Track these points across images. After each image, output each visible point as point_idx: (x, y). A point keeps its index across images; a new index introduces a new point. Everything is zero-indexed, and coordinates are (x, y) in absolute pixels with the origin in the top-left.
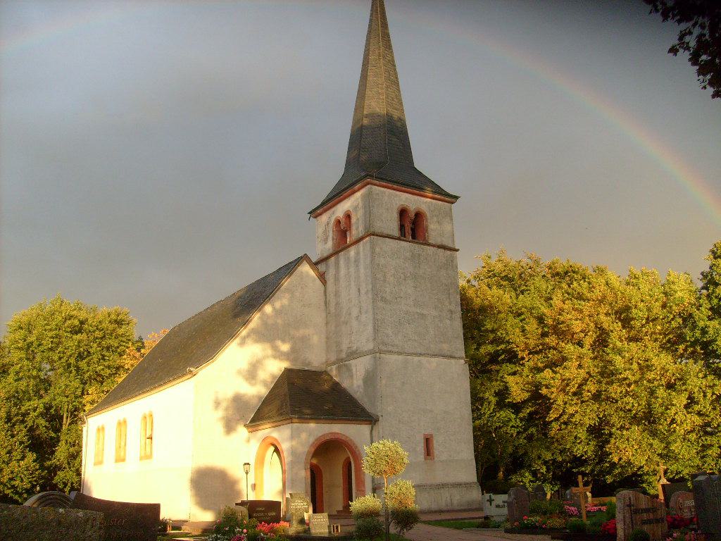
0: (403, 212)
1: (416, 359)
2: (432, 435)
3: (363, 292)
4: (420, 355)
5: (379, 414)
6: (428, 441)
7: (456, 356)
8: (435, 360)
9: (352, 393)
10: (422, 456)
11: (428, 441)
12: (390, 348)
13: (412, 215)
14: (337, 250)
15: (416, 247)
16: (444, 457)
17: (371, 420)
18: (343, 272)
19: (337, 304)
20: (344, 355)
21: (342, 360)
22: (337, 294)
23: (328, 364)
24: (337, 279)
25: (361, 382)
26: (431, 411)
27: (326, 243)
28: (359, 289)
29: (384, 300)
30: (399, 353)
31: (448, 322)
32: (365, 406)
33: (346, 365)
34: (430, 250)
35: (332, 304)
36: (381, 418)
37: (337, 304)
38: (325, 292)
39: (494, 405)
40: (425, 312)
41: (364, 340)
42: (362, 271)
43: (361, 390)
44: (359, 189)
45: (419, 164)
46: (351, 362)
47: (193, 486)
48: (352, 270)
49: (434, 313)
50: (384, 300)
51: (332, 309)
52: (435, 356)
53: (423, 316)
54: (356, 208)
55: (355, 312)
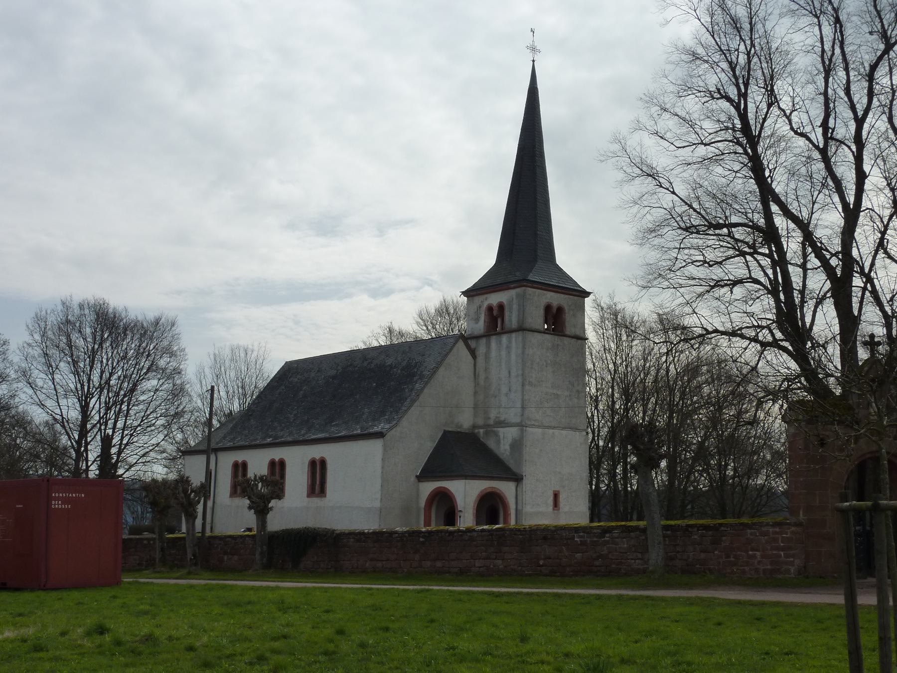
0: (548, 308)
1: (551, 431)
2: (559, 491)
3: (513, 374)
4: (554, 428)
5: (524, 474)
6: (556, 496)
7: (580, 428)
8: (564, 432)
9: (501, 457)
10: (551, 508)
11: (556, 496)
12: (533, 423)
13: (555, 310)
14: (486, 334)
15: (556, 339)
16: (566, 509)
17: (518, 479)
18: (493, 354)
19: (487, 378)
20: (491, 422)
21: (489, 426)
22: (486, 370)
23: (475, 426)
24: (487, 357)
25: (507, 447)
26: (560, 473)
27: (477, 323)
28: (509, 372)
29: (531, 384)
30: (539, 427)
31: (576, 400)
32: (510, 466)
33: (494, 432)
34: (566, 340)
35: (482, 376)
36: (524, 478)
37: (487, 378)
38: (475, 365)
39: (890, 638)
40: (559, 393)
41: (512, 415)
42: (513, 357)
43: (507, 453)
44: (514, 288)
45: (559, 261)
46: (499, 429)
47: (288, 530)
48: (504, 353)
49: (567, 393)
50: (531, 384)
51: (482, 382)
52: (564, 428)
53: (557, 396)
54: (511, 302)
55: (504, 390)
